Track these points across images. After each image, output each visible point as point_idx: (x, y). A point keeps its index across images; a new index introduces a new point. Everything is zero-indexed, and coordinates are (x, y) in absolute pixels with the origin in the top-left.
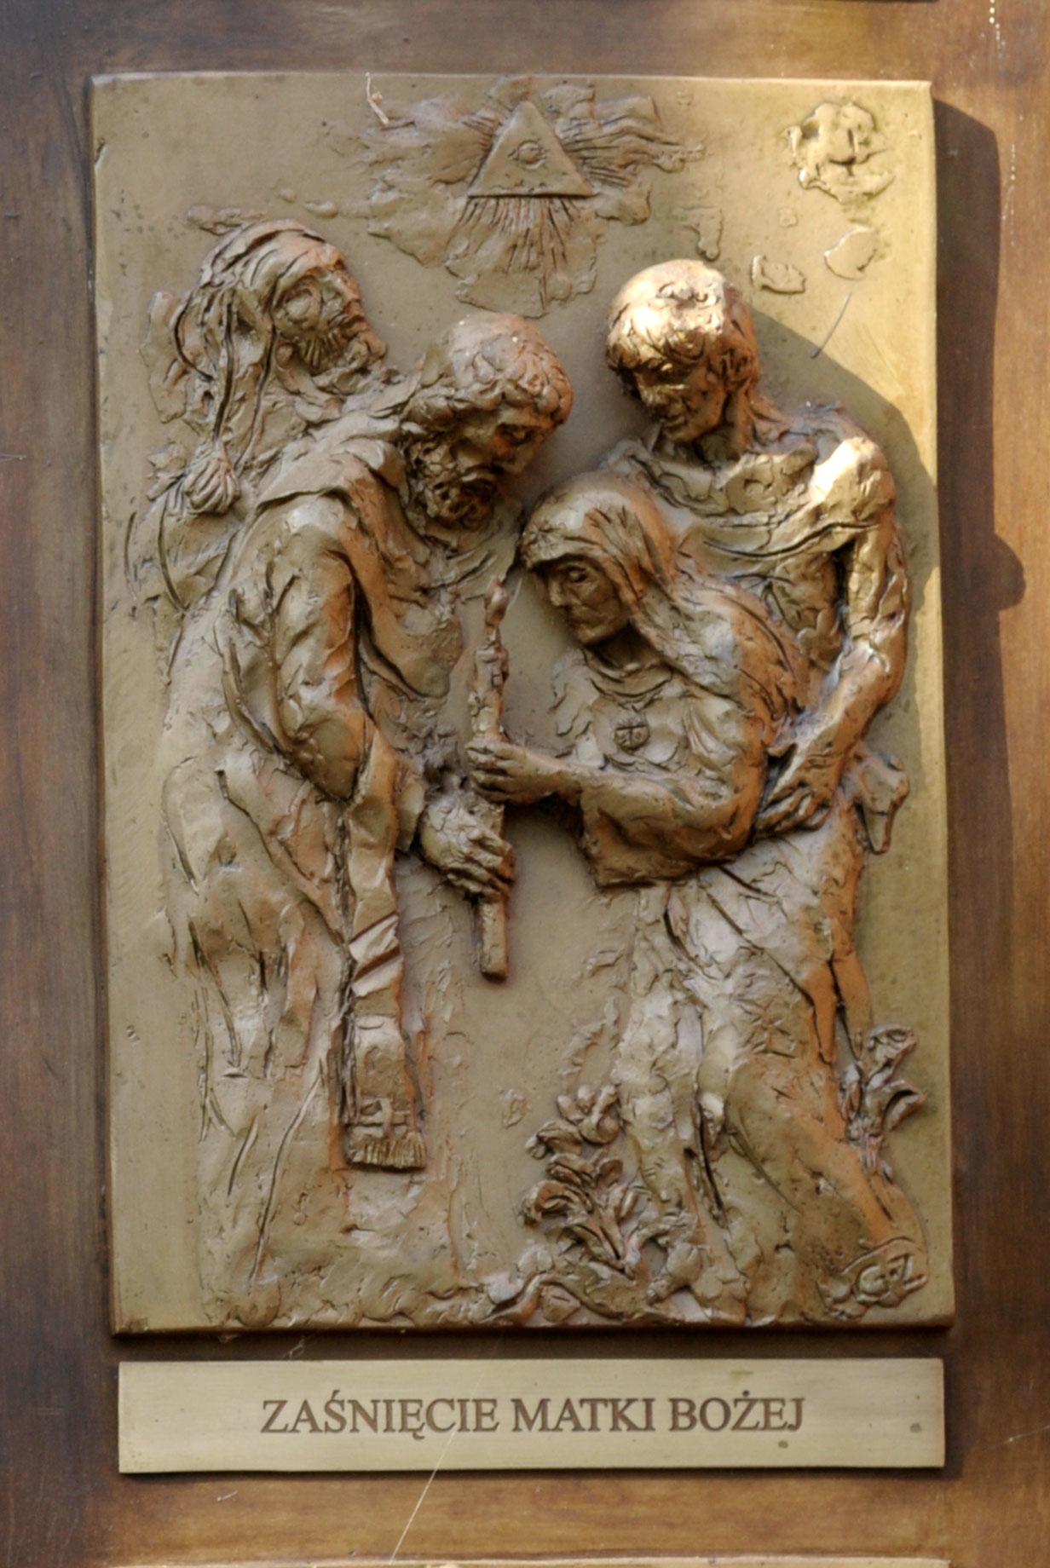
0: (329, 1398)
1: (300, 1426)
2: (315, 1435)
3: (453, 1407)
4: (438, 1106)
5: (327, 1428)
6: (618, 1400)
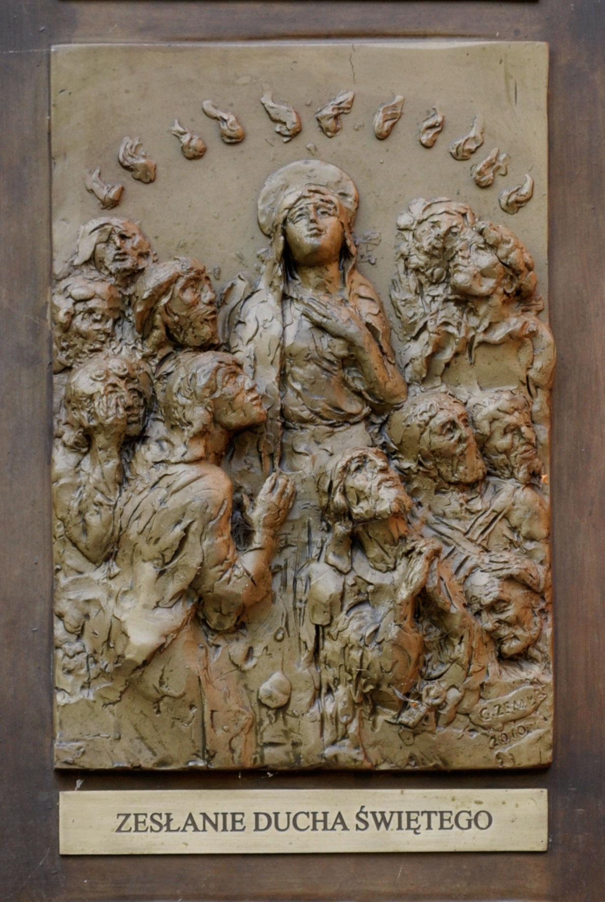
1: (187, 828)
2: (196, 833)
3: (308, 816)
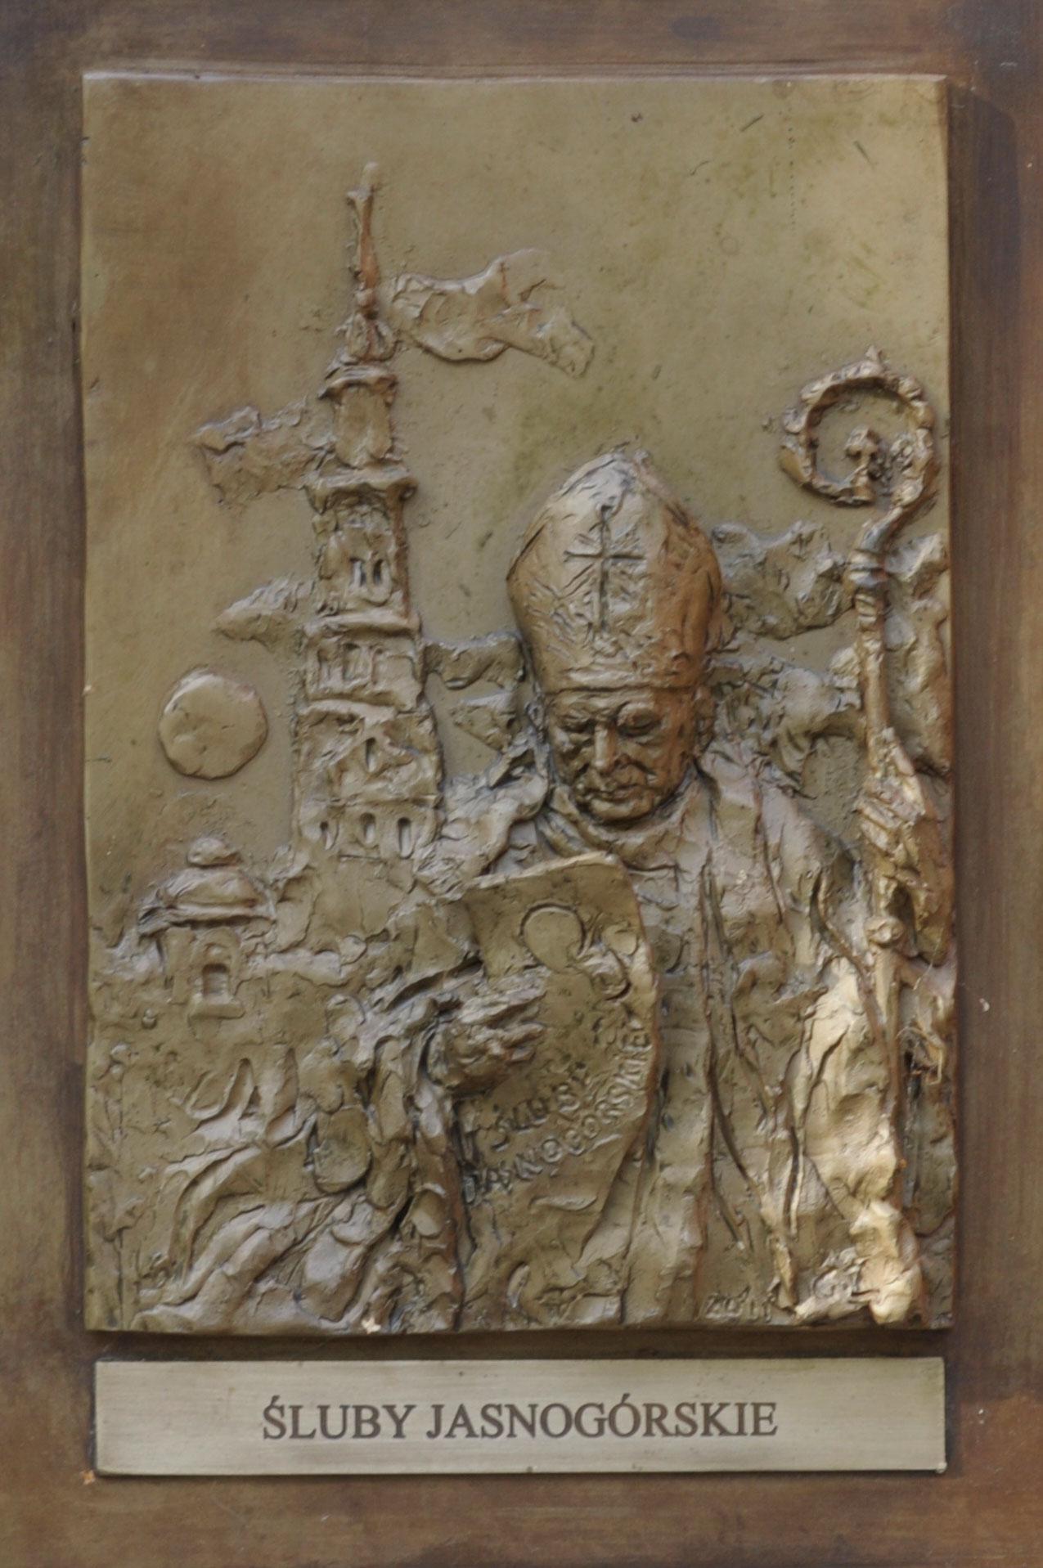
5: (484, 1434)
6: (710, 1405)
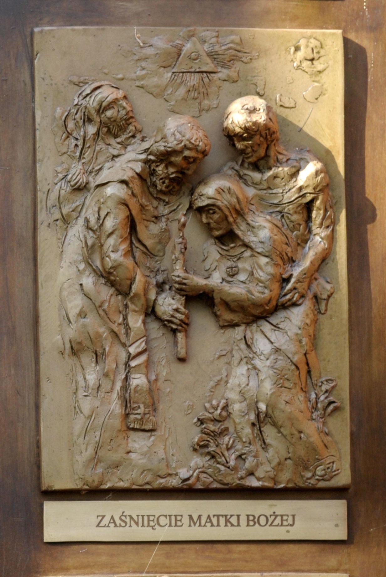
0: (121, 514)
1: (110, 525)
2: (116, 528)
3: (166, 518)
4: (161, 407)
5: (120, 526)
6: (227, 515)
